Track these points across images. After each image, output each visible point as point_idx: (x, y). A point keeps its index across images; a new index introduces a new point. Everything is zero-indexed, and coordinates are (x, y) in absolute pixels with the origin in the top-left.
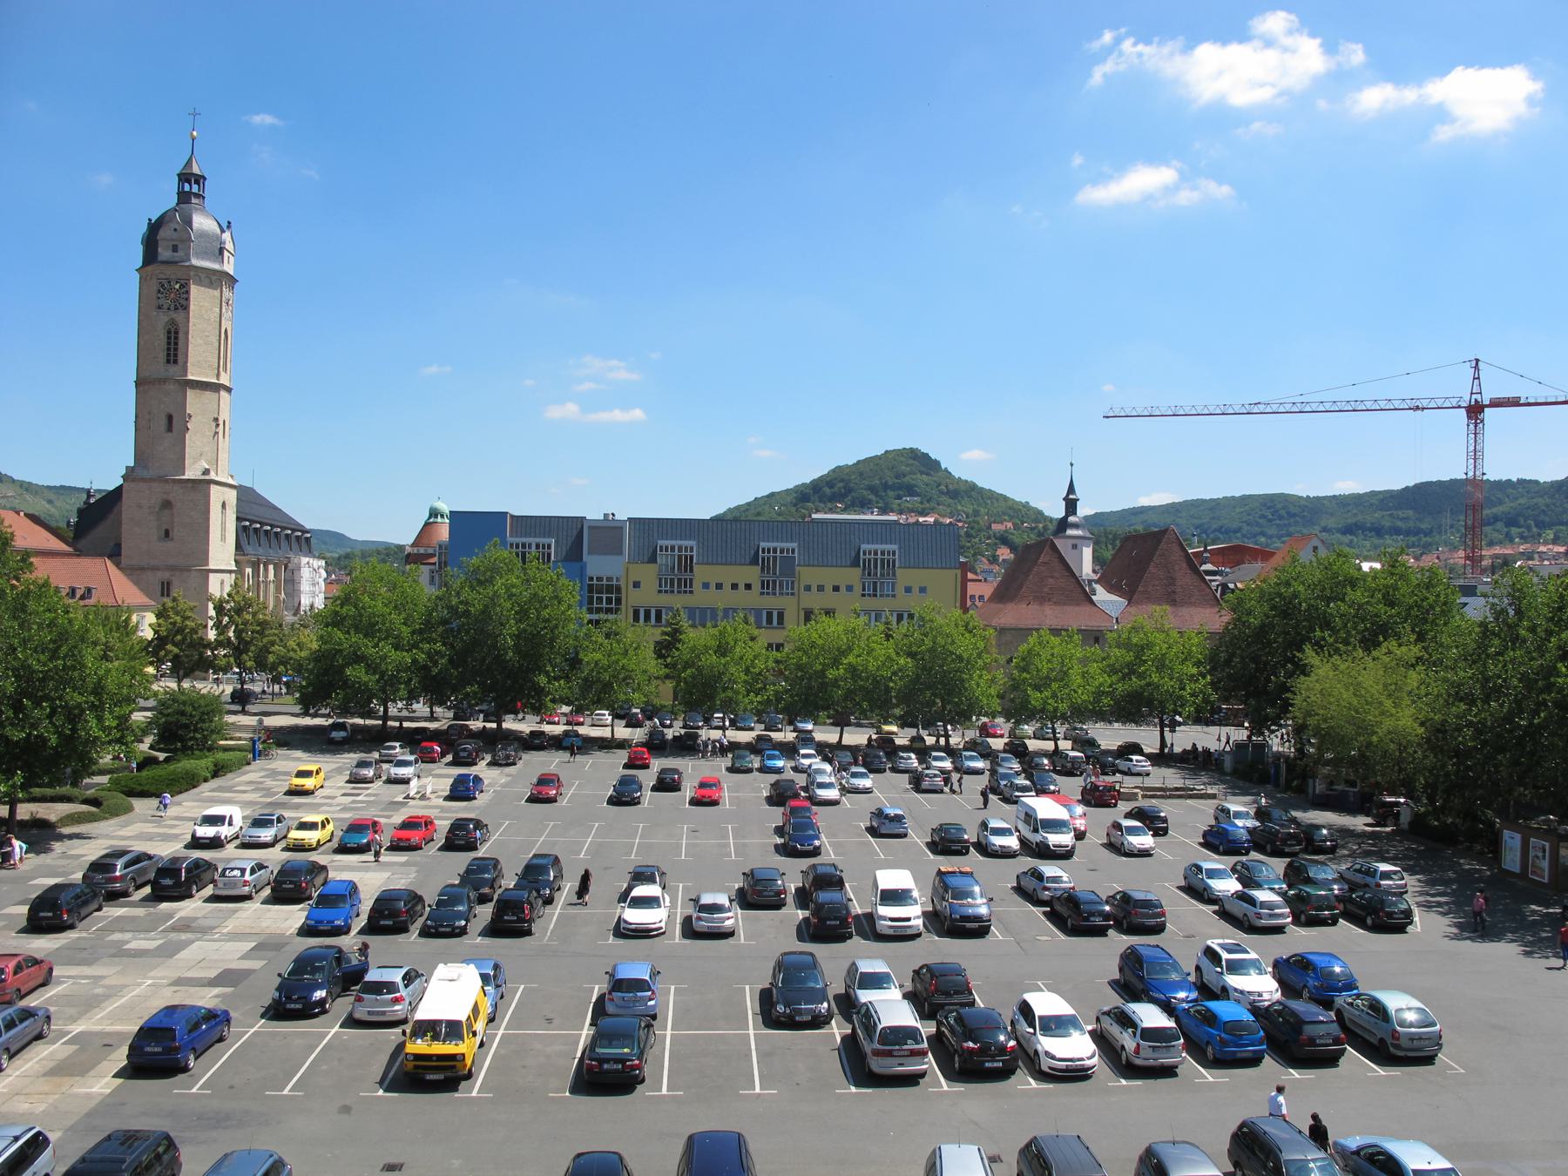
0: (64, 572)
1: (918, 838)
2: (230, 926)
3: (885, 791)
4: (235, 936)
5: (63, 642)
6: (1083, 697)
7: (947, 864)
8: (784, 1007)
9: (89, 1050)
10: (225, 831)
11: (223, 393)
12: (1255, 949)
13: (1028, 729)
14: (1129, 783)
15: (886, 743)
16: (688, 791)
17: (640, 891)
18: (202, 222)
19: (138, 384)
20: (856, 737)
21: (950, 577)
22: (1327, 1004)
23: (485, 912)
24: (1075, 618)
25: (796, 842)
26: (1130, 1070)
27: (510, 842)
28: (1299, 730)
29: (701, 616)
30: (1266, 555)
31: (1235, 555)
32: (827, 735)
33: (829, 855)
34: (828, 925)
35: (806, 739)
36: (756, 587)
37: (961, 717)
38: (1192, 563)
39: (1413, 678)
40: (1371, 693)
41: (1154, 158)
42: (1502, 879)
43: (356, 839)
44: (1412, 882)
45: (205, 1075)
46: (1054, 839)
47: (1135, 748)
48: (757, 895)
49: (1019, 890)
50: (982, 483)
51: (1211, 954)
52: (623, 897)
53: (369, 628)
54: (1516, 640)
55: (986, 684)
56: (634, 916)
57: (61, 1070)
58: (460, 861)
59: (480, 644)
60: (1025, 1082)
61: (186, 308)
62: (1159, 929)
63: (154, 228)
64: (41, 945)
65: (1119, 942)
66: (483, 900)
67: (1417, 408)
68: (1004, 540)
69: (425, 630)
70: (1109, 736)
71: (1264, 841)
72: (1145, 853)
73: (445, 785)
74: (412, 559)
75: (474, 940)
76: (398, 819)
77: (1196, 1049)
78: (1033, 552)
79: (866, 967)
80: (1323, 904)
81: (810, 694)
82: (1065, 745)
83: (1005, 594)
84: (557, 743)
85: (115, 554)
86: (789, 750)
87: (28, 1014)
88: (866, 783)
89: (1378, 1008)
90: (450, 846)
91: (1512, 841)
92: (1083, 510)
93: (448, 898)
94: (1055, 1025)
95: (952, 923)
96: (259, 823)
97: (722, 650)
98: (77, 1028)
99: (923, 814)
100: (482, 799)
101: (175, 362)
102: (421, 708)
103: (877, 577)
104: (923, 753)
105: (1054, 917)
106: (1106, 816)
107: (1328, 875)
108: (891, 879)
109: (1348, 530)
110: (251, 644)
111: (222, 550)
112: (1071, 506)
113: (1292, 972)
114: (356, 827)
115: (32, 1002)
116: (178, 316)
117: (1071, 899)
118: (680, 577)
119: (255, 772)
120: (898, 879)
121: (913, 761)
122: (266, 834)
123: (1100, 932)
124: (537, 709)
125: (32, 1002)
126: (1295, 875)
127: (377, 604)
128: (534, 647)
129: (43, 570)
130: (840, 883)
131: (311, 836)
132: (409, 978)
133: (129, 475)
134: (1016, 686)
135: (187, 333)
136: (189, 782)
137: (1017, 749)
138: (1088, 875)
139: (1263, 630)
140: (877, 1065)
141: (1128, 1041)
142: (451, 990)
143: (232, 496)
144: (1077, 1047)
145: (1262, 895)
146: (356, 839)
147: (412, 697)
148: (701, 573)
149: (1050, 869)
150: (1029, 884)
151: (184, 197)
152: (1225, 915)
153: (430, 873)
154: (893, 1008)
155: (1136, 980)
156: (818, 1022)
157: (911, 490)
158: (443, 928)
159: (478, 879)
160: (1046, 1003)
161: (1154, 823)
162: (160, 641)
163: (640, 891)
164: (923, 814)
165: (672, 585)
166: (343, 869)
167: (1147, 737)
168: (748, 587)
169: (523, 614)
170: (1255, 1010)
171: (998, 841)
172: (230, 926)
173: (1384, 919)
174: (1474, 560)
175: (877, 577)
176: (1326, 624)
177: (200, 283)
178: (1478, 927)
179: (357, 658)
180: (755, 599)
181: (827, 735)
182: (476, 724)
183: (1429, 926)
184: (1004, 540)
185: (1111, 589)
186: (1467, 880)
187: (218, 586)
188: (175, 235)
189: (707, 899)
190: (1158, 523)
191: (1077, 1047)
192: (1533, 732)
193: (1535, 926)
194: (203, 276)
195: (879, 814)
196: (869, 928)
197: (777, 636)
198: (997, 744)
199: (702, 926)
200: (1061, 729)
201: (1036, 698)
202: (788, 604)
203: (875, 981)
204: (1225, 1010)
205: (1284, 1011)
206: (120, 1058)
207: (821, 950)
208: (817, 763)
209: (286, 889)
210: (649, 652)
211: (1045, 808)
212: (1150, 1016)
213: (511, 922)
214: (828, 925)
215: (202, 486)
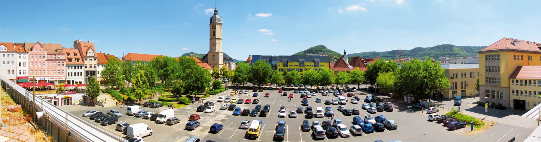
0: (201, 65)
1: (323, 102)
2: (223, 113)
3: (318, 95)
4: (223, 115)
5: (202, 73)
6: (347, 81)
7: (327, 106)
8: (304, 128)
9: (204, 129)
10: (222, 100)
12: (373, 116)
13: (339, 86)
14: (354, 93)
15: (318, 89)
16: (288, 96)
17: (282, 110)
18: (218, 16)
20: (314, 88)
21: (327, 63)
22: (382, 123)
23: (259, 113)
24: (346, 69)
25: (304, 103)
26: (355, 135)
27: (262, 103)
28: (377, 84)
29: (289, 70)
30: (373, 60)
31: (368, 60)
32: (309, 87)
33: (310, 105)
34: (309, 115)
35: (306, 88)
37: (329, 84)
38: (362, 61)
39: (393, 76)
40: (386, 79)
41: (356, 4)
42: (404, 103)
43: (240, 102)
44: (393, 104)
45: (220, 133)
46: (343, 102)
47: (355, 88)
48: (299, 111)
49: (338, 109)
50: (332, 50)
51: (366, 117)
52: (279, 111)
53: (241, 72)
54: (404, 71)
55: (333, 79)
56: (281, 114)
57: (201, 131)
58: (255, 105)
59: (257, 75)
60: (339, 138)
62: (358, 114)
63: (211, 18)
64: (199, 113)
65: (353, 116)
66: (259, 111)
68: (335, 58)
69: (249, 72)
70: (351, 86)
71: (373, 100)
72: (356, 103)
73: (252, 95)
74: (247, 62)
75: (257, 117)
76: (246, 99)
77: (364, 131)
78: (339, 61)
79: (315, 122)
80: (381, 109)
81: (307, 81)
82: (345, 88)
83: (335, 66)
84: (268, 89)
85: (207, 62)
86: (304, 90)
87: (197, 122)
88: (315, 94)
89: (389, 123)
90: (253, 103)
91: (405, 98)
92: (347, 54)
93: (254, 111)
94: (343, 129)
95: (328, 115)
96: (227, 99)
97: (293, 75)
98: (203, 125)
99: (324, 99)
100: (258, 97)
102: (249, 83)
103: (316, 64)
104: (324, 90)
105: (343, 113)
106: (350, 98)
107: (382, 104)
108: (319, 109)
109: (384, 57)
110: (225, 75)
111: (221, 61)
112: (345, 53)
113: (378, 119)
114: (240, 100)
115: (198, 121)
117: (346, 111)
118: (286, 65)
119: (226, 92)
120: (320, 108)
121: (322, 91)
122: (228, 101)
123: (350, 115)
124: (266, 84)
125: (198, 121)
126: (377, 105)
127: (242, 69)
128: (265, 74)
129: (198, 64)
130: (311, 109)
131: (234, 101)
132: (248, 122)
133: (209, 52)
134: (337, 79)
135: (479, 47)
136: (217, 93)
137: (338, 89)
138: (349, 107)
139: (372, 70)
140: (317, 137)
141: (354, 131)
142: (255, 124)
144: (347, 132)
145: (373, 108)
146: (240, 102)
147: (247, 82)
148: (289, 64)
149: (342, 106)
150: (340, 109)
151: (215, 14)
152: (368, 111)
153: (251, 107)
154: (319, 128)
155: (355, 122)
156: (308, 131)
157: (321, 51)
158: (253, 115)
159: (258, 108)
160: (342, 126)
161: (358, 99)
162: (213, 74)
163: (282, 110)
164: (324, 99)
166: (238, 106)
167: (356, 86)
169: (263, 70)
170: (372, 125)
171: (335, 102)
172: (223, 113)
173: (389, 110)
174: (400, 61)
175: (316, 64)
176: (381, 69)
178: (401, 110)
179: (240, 76)
180: (298, 67)
181: (309, 87)
182: (257, 86)
183: (395, 110)
184: (335, 58)
185: (351, 65)
186: (400, 104)
187: (221, 66)
189: (292, 112)
190: (358, 55)
191: (347, 132)
192: (407, 83)
193: (408, 109)
195: (317, 99)
196: (316, 116)
197: (301, 73)
198: (335, 88)
199: (291, 116)
200: (344, 86)
201: (340, 81)
202: (303, 68)
203: (317, 124)
204: (368, 125)
205: (376, 124)
206: (209, 130)
207: (309, 120)
208: (308, 91)
209: (231, 108)
210: (282, 75)
211: (342, 97)
212: (357, 127)
213: (263, 115)
214: (309, 115)
215: (218, 53)
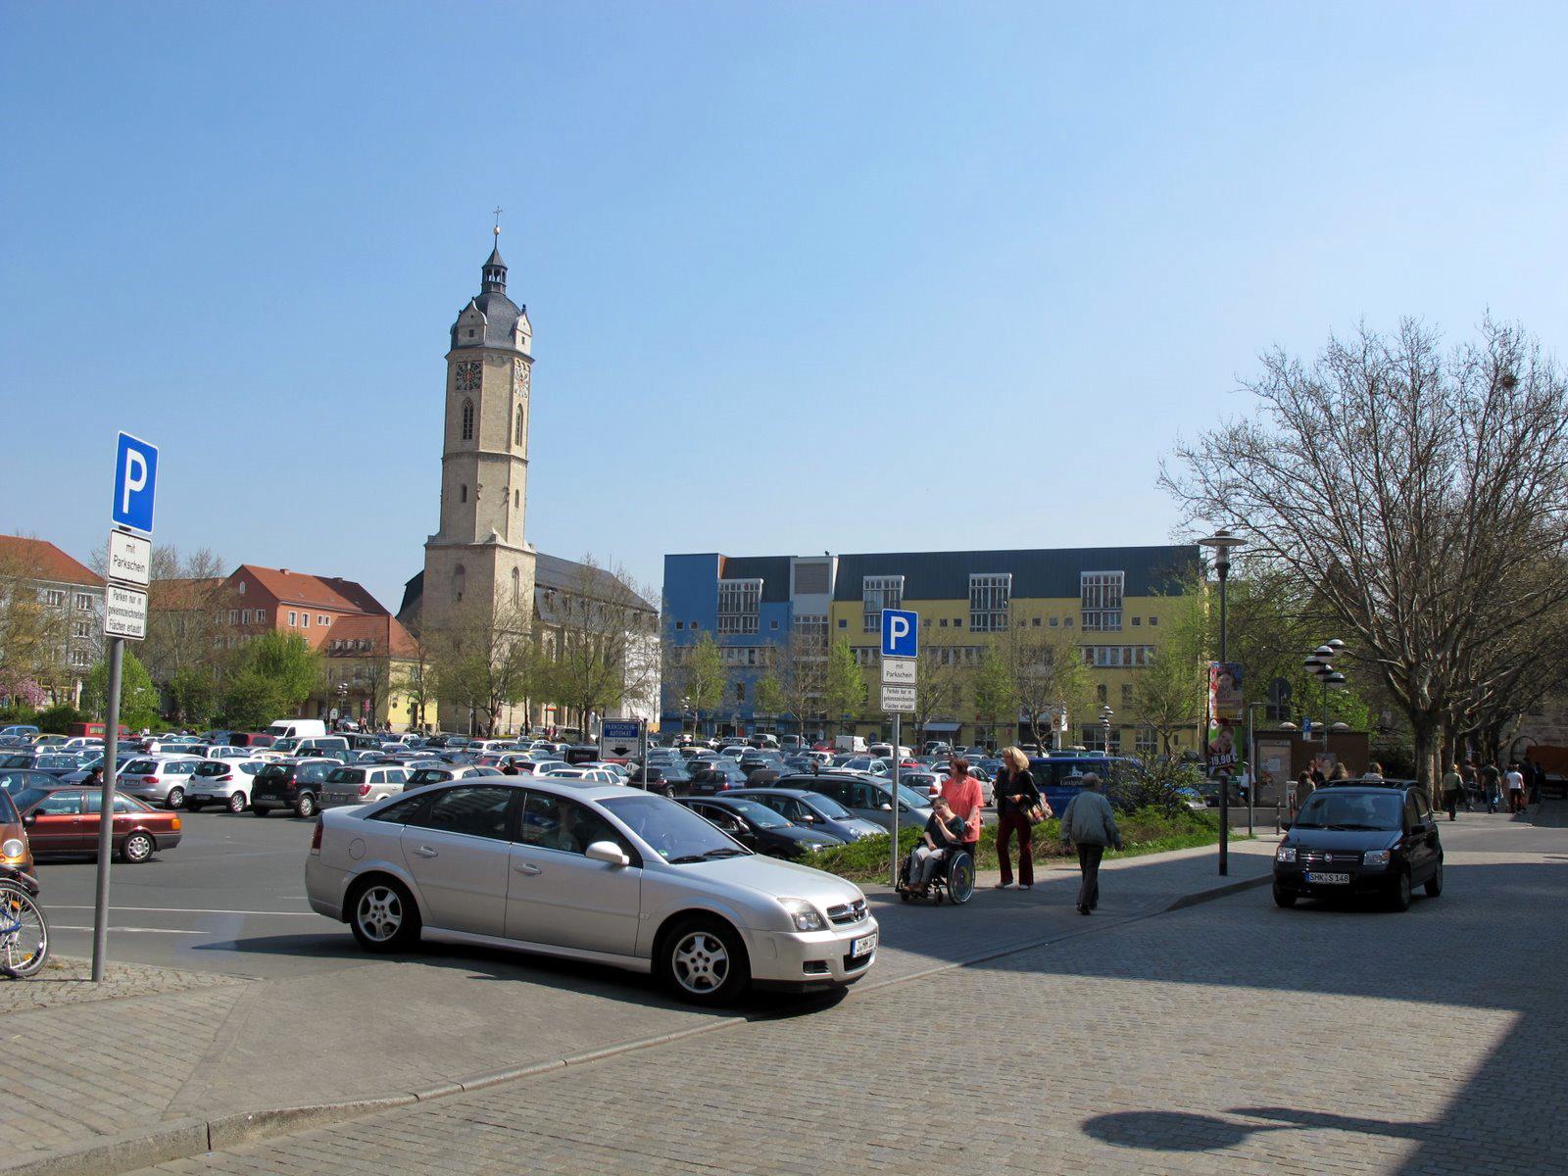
11: (514, 465)
19: (444, 460)
36: (966, 624)
61: (479, 387)
67: (280, 1162)
101: (470, 437)
116: (472, 395)
143: (529, 566)
165: (985, 624)
168: (958, 622)
177: (492, 362)
188: (471, 322)
194: (495, 356)
